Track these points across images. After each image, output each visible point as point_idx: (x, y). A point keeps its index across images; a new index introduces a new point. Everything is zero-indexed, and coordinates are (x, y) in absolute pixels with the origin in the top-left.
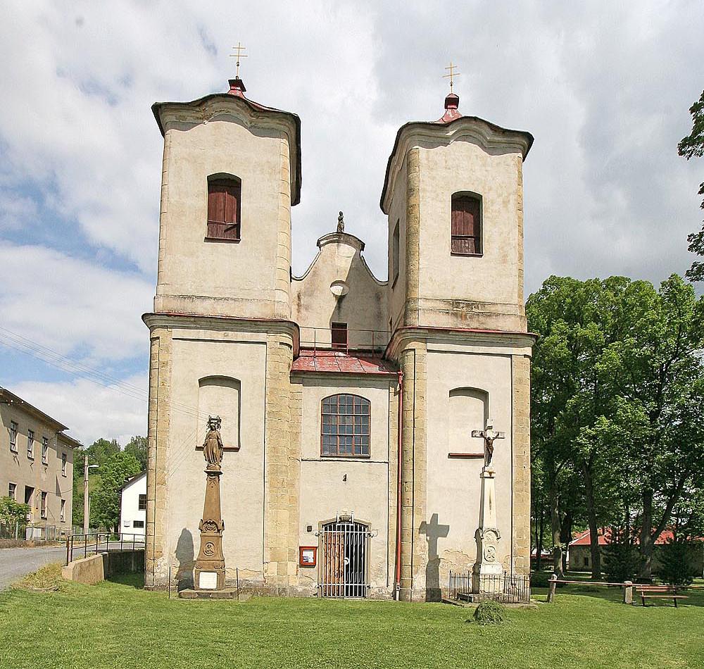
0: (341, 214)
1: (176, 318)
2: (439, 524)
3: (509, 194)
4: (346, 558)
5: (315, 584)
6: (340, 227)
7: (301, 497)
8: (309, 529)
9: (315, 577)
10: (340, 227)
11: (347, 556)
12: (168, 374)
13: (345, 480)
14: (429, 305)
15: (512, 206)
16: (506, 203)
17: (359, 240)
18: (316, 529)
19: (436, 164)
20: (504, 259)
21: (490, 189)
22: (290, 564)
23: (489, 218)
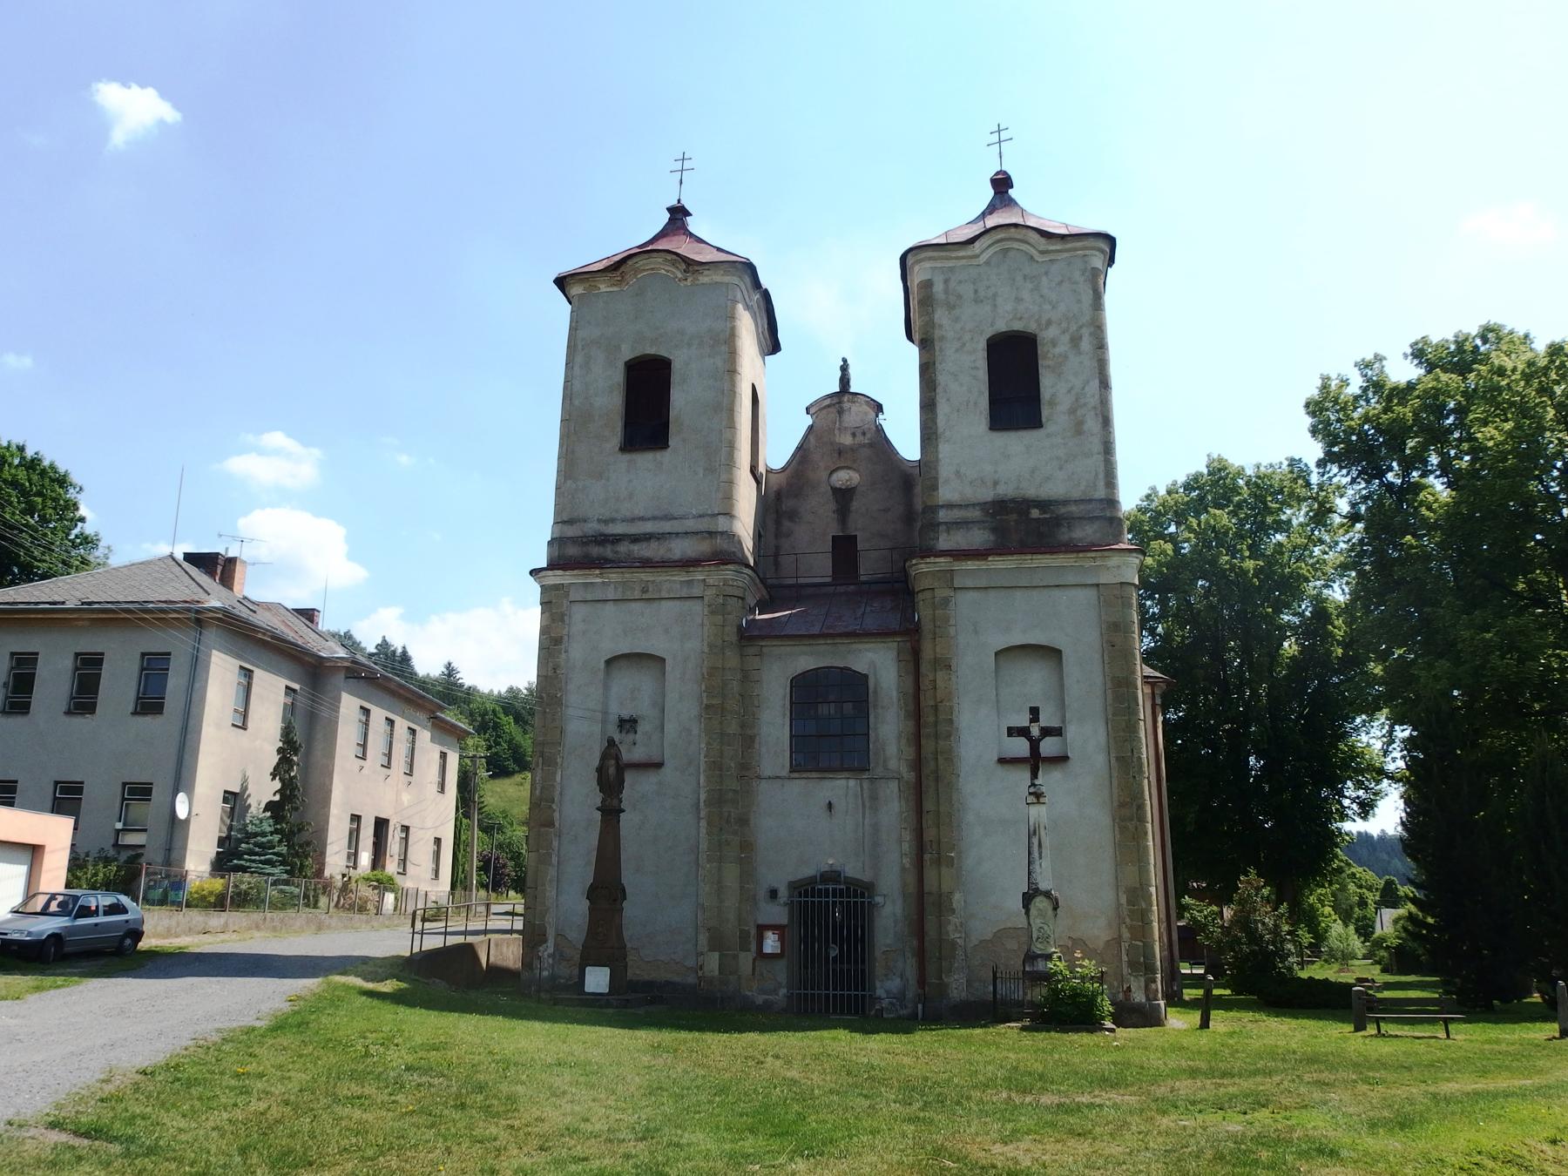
0: (845, 360)
1: (977, 244)
2: (606, 971)
3: (1081, 327)
4: (831, 945)
5: (783, 991)
6: (845, 381)
7: (220, 1026)
8: (773, 894)
9: (782, 977)
10: (845, 381)
11: (835, 943)
12: (563, 656)
13: (830, 805)
14: (956, 514)
15: (1086, 345)
16: (1075, 341)
17: (872, 400)
18: (783, 893)
19: (960, 297)
20: (1078, 429)
21: (1049, 323)
22: (742, 955)
23: (1049, 367)
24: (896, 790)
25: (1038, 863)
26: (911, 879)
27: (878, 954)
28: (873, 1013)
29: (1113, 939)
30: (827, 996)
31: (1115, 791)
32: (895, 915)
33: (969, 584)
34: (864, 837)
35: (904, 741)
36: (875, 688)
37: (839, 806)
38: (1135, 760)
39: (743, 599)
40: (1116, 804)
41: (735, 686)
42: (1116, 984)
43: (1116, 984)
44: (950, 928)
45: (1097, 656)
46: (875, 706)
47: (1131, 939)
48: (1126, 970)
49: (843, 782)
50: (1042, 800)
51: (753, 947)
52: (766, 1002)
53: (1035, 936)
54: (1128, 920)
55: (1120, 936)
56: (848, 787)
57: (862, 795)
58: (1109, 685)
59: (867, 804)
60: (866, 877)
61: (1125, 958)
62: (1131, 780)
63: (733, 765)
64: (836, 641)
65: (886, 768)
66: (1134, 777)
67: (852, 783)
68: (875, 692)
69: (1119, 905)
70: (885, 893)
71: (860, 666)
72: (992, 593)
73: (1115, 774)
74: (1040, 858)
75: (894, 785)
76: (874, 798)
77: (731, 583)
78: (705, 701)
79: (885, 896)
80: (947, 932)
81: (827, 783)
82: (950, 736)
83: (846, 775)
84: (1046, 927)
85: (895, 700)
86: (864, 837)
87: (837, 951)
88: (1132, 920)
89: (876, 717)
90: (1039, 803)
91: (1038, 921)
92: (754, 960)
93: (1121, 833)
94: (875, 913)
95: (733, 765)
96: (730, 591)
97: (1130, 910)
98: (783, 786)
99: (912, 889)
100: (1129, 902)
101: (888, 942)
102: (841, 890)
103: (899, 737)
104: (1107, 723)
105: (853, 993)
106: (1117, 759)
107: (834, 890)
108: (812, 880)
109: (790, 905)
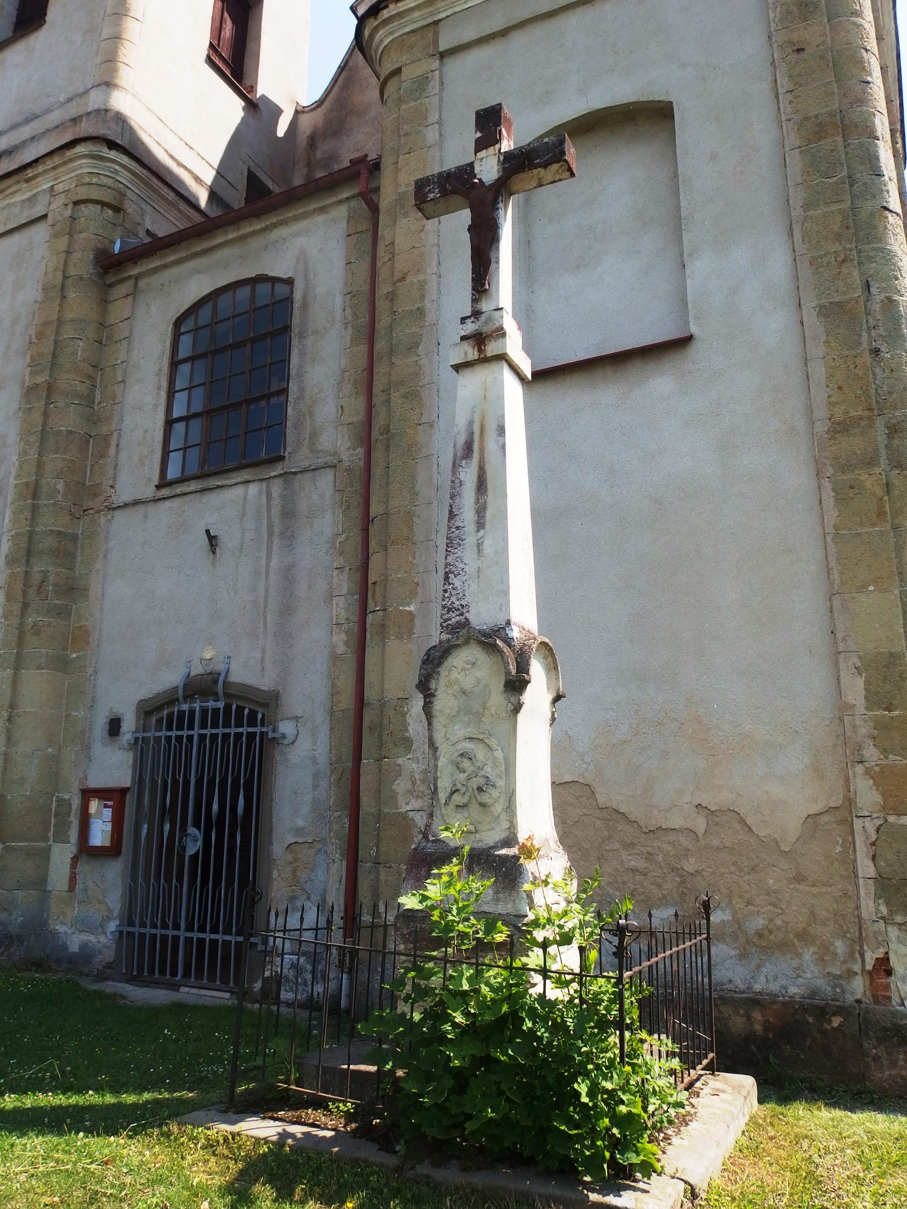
4: (192, 830)
5: (112, 926)
8: (114, 727)
11: (197, 825)
24: (329, 492)
25: (470, 541)
26: (347, 682)
27: (278, 850)
28: (258, 985)
29: (830, 810)
30: (176, 939)
31: (820, 396)
32: (314, 760)
33: (469, 34)
34: (266, 597)
35: (348, 388)
36: (305, 298)
37: (229, 540)
38: (877, 307)
39: (117, 209)
40: (821, 428)
41: (81, 350)
42: (840, 946)
43: (840, 946)
44: (401, 786)
45: (761, 90)
46: (302, 335)
47: (886, 809)
48: (869, 906)
49: (239, 491)
50: (492, 349)
51: (74, 834)
52: (84, 946)
53: (444, 785)
54: (871, 752)
55: (850, 802)
56: (245, 499)
57: (269, 510)
58: (793, 139)
59: (277, 530)
60: (265, 683)
61: (866, 868)
62: (867, 358)
63: (60, 487)
64: (242, 232)
65: (314, 451)
66: (876, 352)
67: (253, 489)
68: (305, 306)
69: (844, 709)
70: (299, 713)
71: (279, 268)
72: (518, 39)
73: (817, 350)
74: (480, 524)
75: (326, 481)
76: (288, 514)
77: (87, 180)
78: (27, 384)
79: (297, 718)
80: (394, 797)
81: (214, 499)
82: (417, 344)
83: (244, 475)
84: (480, 753)
85: (338, 313)
86: (266, 597)
87: (200, 843)
88: (885, 752)
89: (302, 354)
90: (484, 360)
91: (459, 731)
92: (75, 860)
93: (841, 501)
94: (278, 757)
95: (60, 487)
96: (83, 193)
97: (878, 724)
98: (146, 517)
99: (347, 701)
100: (873, 699)
101: (300, 823)
102: (216, 711)
103: (340, 385)
104: (791, 234)
105: (196, 935)
106: (824, 311)
107: (204, 711)
108: (169, 699)
109: (140, 746)
